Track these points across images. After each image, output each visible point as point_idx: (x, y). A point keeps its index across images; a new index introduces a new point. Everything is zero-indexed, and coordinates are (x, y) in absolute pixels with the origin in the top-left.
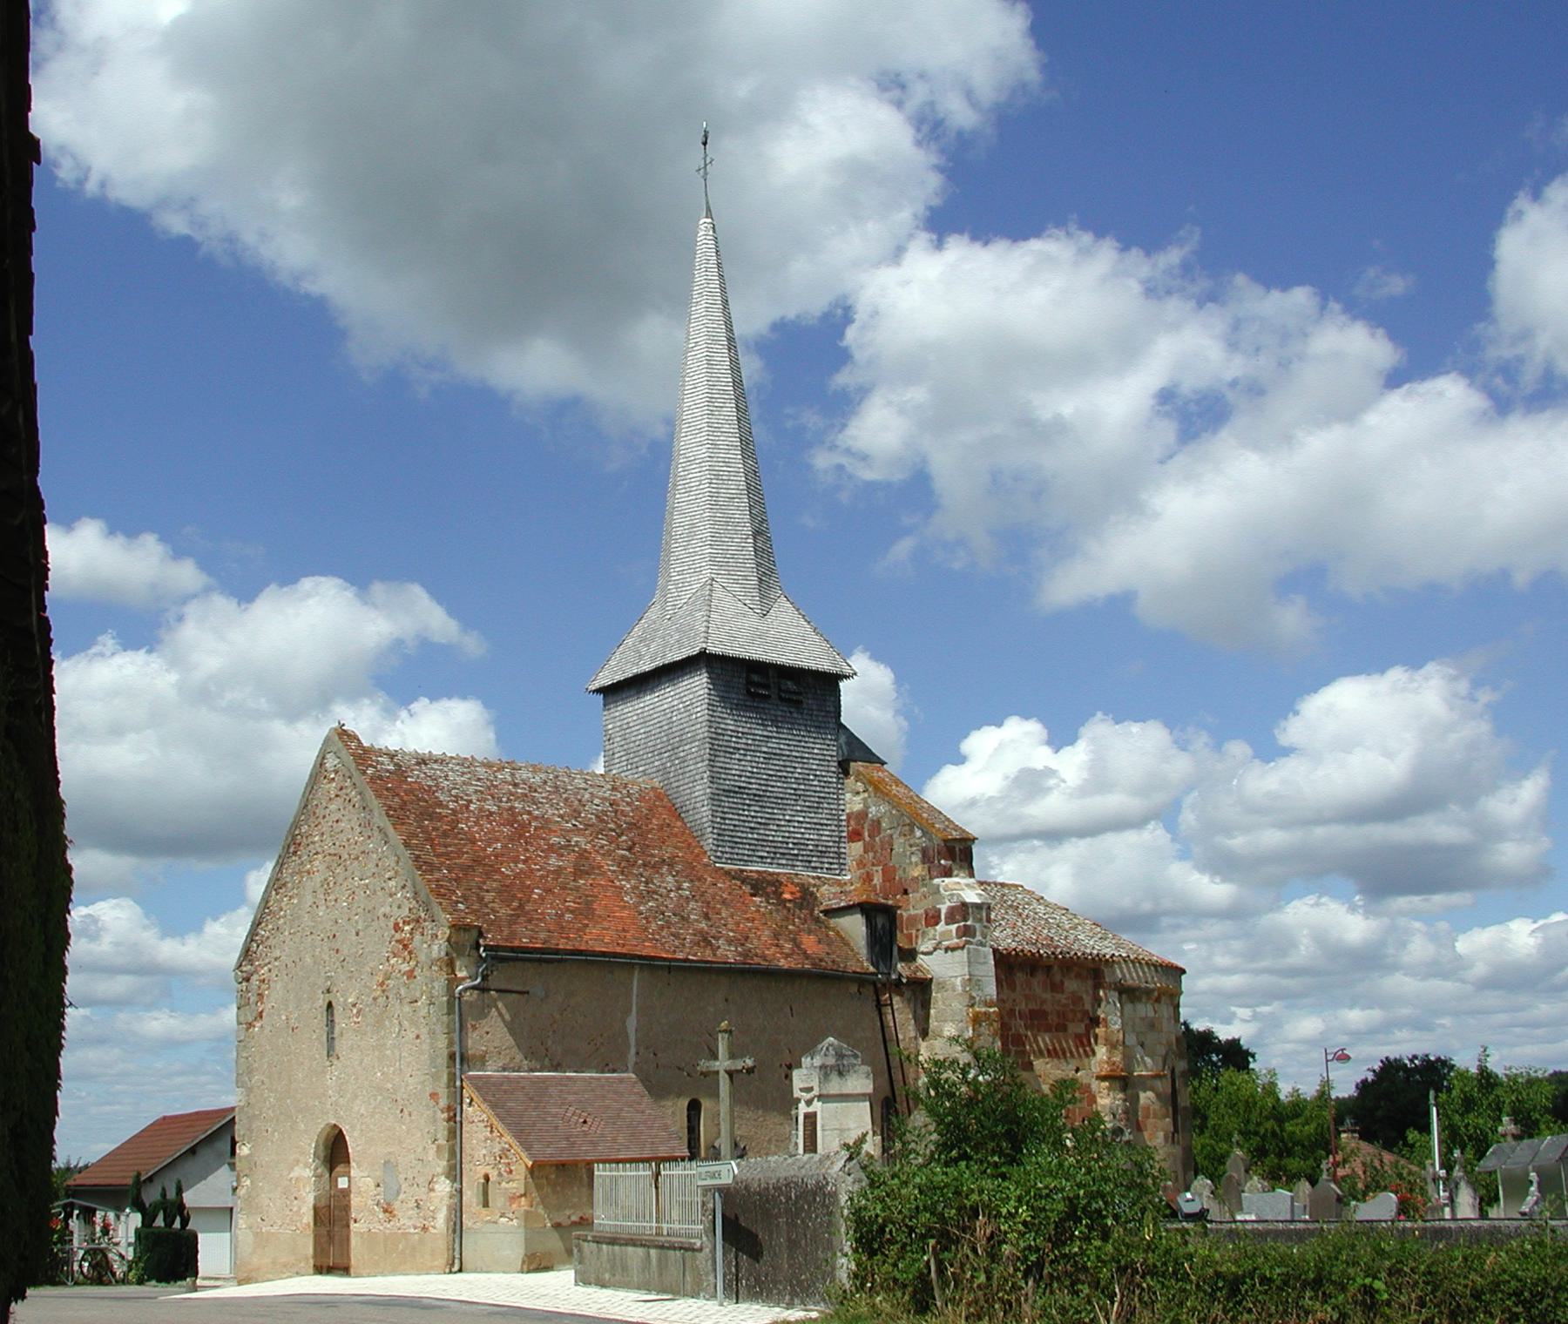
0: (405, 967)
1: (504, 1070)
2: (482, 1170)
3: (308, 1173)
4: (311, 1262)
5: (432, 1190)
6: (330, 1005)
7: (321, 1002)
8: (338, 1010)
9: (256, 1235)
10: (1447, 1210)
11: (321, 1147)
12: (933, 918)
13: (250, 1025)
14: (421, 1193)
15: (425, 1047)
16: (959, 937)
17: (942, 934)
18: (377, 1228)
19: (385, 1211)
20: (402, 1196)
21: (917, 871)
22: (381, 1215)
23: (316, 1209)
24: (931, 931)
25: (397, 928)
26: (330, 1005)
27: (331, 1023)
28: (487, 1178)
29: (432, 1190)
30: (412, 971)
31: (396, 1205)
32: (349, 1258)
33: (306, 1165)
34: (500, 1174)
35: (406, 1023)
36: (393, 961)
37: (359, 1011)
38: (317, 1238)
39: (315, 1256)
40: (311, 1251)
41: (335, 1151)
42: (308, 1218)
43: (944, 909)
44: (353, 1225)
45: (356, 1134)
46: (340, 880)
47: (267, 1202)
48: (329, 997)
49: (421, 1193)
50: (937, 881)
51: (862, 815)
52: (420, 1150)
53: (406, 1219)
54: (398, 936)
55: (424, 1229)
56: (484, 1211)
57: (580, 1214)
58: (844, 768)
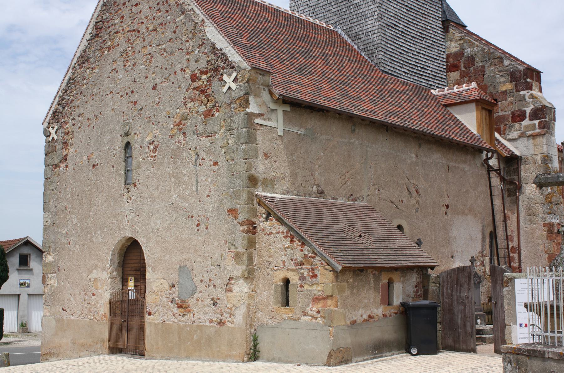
0: (203, 108)
1: (288, 192)
2: (281, 275)
3: (105, 275)
4: (107, 344)
5: (230, 290)
6: (128, 145)
7: (119, 145)
8: (135, 147)
9: (58, 321)
10: (485, 287)
11: (117, 256)
12: (519, 117)
13: (56, 166)
14: (219, 293)
15: (224, 171)
16: (540, 128)
17: (526, 127)
18: (170, 320)
19: (180, 307)
20: (197, 295)
21: (509, 86)
22: (176, 311)
23: (111, 302)
24: (517, 125)
25: (194, 78)
26: (128, 145)
27: (128, 158)
28: (287, 282)
29: (230, 290)
30: (210, 111)
31: (192, 302)
32: (144, 344)
33: (104, 269)
34: (302, 278)
35: (203, 155)
36: (190, 105)
37: (156, 147)
38: (111, 325)
39: (110, 340)
40: (106, 335)
41: (131, 259)
42: (104, 309)
43: (528, 110)
44: (147, 317)
45: (151, 244)
46: (138, 48)
47: (68, 296)
48: (126, 139)
49: (219, 293)
50: (522, 93)
51: (460, 54)
52: (217, 255)
53: (202, 313)
54: (195, 84)
55: (221, 323)
56: (284, 310)
57: (368, 313)
58: (446, 30)
